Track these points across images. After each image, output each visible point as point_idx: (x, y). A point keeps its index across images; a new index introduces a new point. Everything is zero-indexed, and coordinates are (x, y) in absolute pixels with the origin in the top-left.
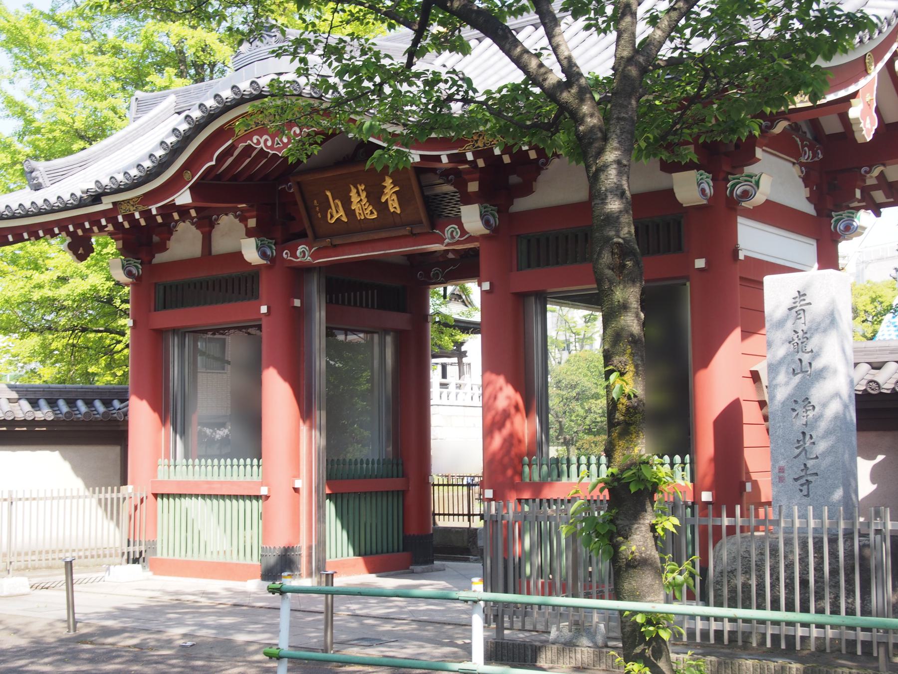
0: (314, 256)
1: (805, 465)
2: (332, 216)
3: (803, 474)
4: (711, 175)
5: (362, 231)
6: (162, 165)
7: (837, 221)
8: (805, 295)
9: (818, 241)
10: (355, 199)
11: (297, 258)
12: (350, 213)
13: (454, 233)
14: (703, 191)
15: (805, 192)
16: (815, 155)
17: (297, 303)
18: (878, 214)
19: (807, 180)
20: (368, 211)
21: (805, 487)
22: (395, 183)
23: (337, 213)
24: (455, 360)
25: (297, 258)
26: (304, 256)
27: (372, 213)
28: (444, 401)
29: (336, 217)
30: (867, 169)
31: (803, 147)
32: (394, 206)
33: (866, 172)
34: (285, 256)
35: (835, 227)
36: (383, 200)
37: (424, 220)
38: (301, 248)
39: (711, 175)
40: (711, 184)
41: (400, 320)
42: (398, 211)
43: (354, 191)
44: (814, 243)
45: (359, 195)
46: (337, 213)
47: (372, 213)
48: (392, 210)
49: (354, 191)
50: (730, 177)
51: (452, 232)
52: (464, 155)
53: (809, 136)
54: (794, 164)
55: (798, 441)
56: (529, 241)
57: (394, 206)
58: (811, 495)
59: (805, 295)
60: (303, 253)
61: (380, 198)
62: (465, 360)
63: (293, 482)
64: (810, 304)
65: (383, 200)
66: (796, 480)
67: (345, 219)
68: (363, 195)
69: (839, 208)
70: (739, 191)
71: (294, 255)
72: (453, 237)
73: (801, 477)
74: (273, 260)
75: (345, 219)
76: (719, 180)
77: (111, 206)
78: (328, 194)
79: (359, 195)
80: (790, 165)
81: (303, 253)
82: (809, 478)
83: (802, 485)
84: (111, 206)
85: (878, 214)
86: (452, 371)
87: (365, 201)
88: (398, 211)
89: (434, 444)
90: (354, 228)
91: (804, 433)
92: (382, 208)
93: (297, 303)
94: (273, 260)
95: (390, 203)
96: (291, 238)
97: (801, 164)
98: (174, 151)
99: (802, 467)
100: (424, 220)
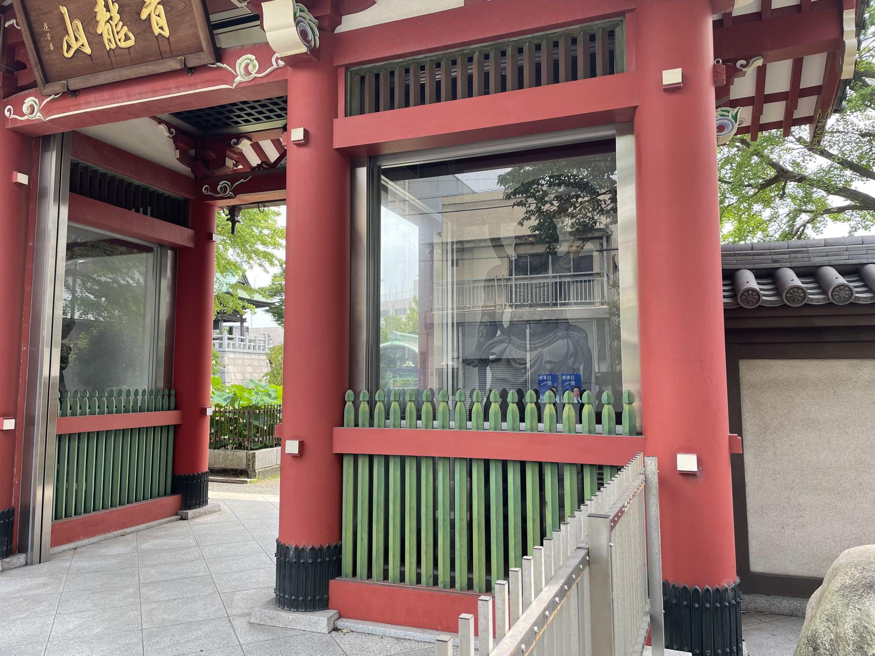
0: (45, 111)
2: (69, 47)
11: (23, 115)
12: (95, 39)
13: (250, 68)
17: (23, 179)
20: (122, 35)
23: (76, 40)
24: (238, 324)
25: (23, 115)
26: (32, 112)
27: (127, 38)
28: (231, 349)
29: (75, 46)
30: (744, 62)
32: (160, 24)
33: (742, 66)
34: (7, 114)
36: (144, 16)
37: (204, 44)
38: (30, 101)
41: (181, 235)
42: (166, 33)
45: (108, 10)
46: (76, 40)
47: (127, 38)
48: (157, 31)
51: (248, 65)
56: (363, 79)
57: (160, 24)
61: (139, 14)
62: (245, 324)
63: (183, 417)
65: (144, 16)
67: (88, 50)
72: (248, 73)
75: (88, 50)
78: (64, 10)
79: (108, 10)
86: (236, 334)
87: (117, 17)
88: (166, 33)
89: (841, 367)
90: (102, 59)
92: (142, 27)
93: (23, 179)
95: (154, 18)
100: (204, 44)
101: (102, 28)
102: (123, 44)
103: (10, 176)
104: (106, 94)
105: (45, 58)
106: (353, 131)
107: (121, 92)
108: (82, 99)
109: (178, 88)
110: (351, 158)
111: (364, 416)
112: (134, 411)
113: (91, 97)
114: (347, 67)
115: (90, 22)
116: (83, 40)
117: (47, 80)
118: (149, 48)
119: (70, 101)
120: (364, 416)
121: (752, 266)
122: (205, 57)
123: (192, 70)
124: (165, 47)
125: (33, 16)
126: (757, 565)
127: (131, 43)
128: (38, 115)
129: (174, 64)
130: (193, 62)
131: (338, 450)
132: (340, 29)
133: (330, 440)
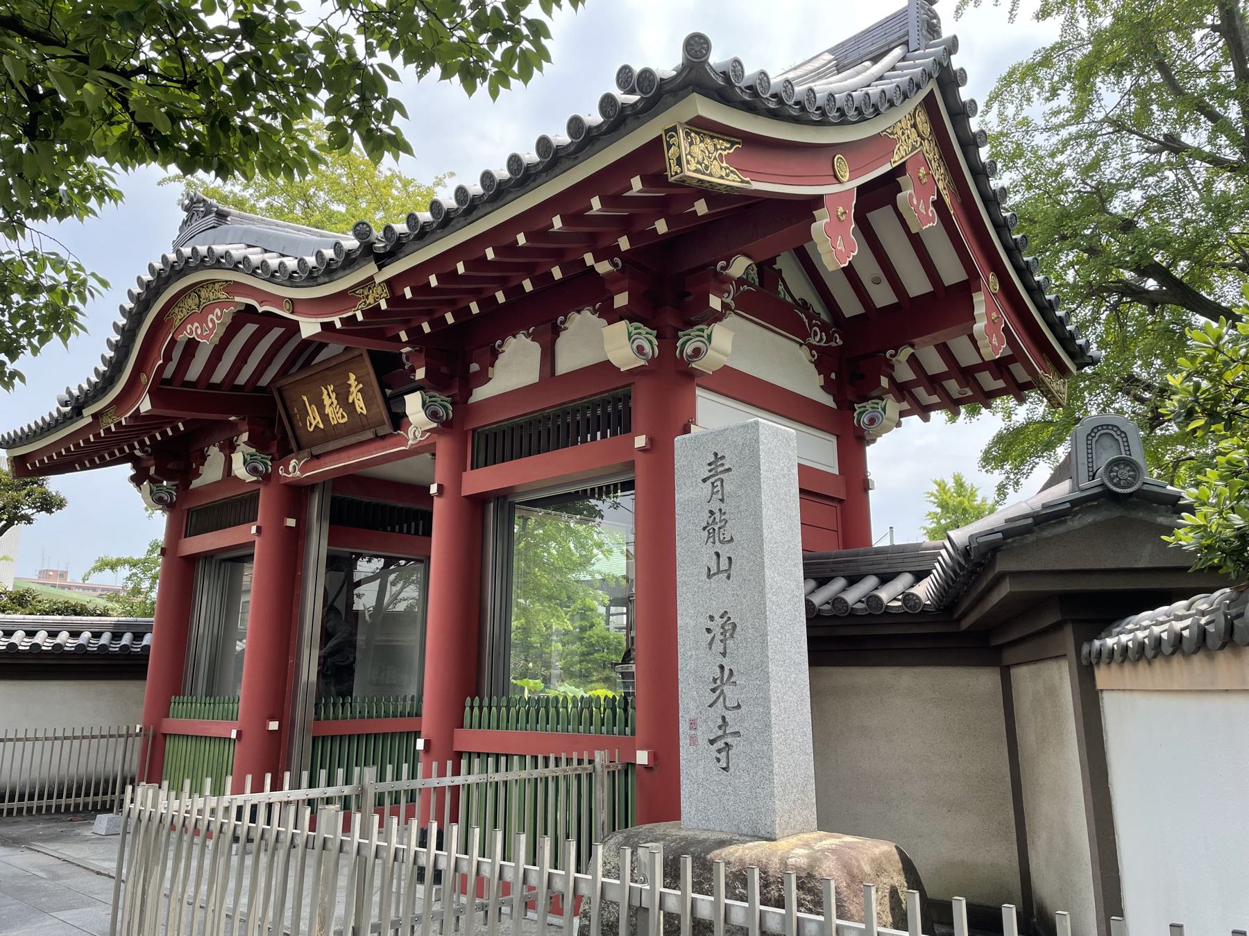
0: (302, 470)
1: (724, 718)
3: (720, 733)
4: (655, 332)
5: (336, 437)
6: (115, 367)
7: (861, 414)
8: (723, 457)
9: (838, 437)
10: (327, 402)
12: (325, 418)
14: (640, 350)
15: (819, 380)
16: (830, 339)
17: (291, 522)
18: (926, 419)
19: (820, 365)
21: (724, 754)
22: (358, 380)
23: (314, 420)
29: (314, 423)
31: (811, 326)
32: (360, 406)
35: (859, 421)
38: (293, 462)
39: (655, 332)
40: (655, 342)
42: (365, 412)
43: (325, 392)
44: (834, 440)
48: (359, 410)
49: (325, 392)
50: (680, 333)
52: (355, 316)
53: (824, 317)
54: (801, 345)
55: (715, 680)
57: (360, 406)
58: (732, 770)
59: (723, 457)
60: (294, 469)
64: (729, 470)
66: (712, 742)
67: (321, 426)
68: (333, 396)
69: (864, 399)
70: (689, 350)
71: (287, 471)
72: (415, 437)
73: (719, 737)
74: (266, 478)
75: (321, 426)
76: (667, 338)
77: (90, 420)
80: (797, 346)
81: (294, 469)
82: (729, 740)
83: (719, 751)
84: (90, 420)
85: (926, 419)
88: (365, 412)
89: (885, 675)
90: (330, 433)
91: (722, 667)
92: (350, 408)
93: (291, 522)
94: (266, 478)
96: (283, 453)
97: (811, 347)
98: (122, 349)
99: (720, 722)
101: (328, 410)
102: (341, 421)
103: (283, 521)
104: (335, 457)
105: (298, 432)
106: (480, 480)
107: (344, 455)
108: (323, 460)
109: (377, 451)
110: (478, 502)
111: (494, 723)
112: (395, 716)
113: (327, 459)
114: (474, 430)
115: (321, 407)
116: (318, 419)
117: (300, 448)
118: (357, 424)
119: (315, 462)
120: (494, 723)
121: (847, 573)
122: (387, 429)
123: (383, 437)
124: (365, 422)
125: (288, 404)
126: (169, 744)
127: (345, 420)
128: (298, 473)
129: (369, 435)
130: (381, 433)
131: (457, 748)
132: (472, 400)
133: (450, 739)
